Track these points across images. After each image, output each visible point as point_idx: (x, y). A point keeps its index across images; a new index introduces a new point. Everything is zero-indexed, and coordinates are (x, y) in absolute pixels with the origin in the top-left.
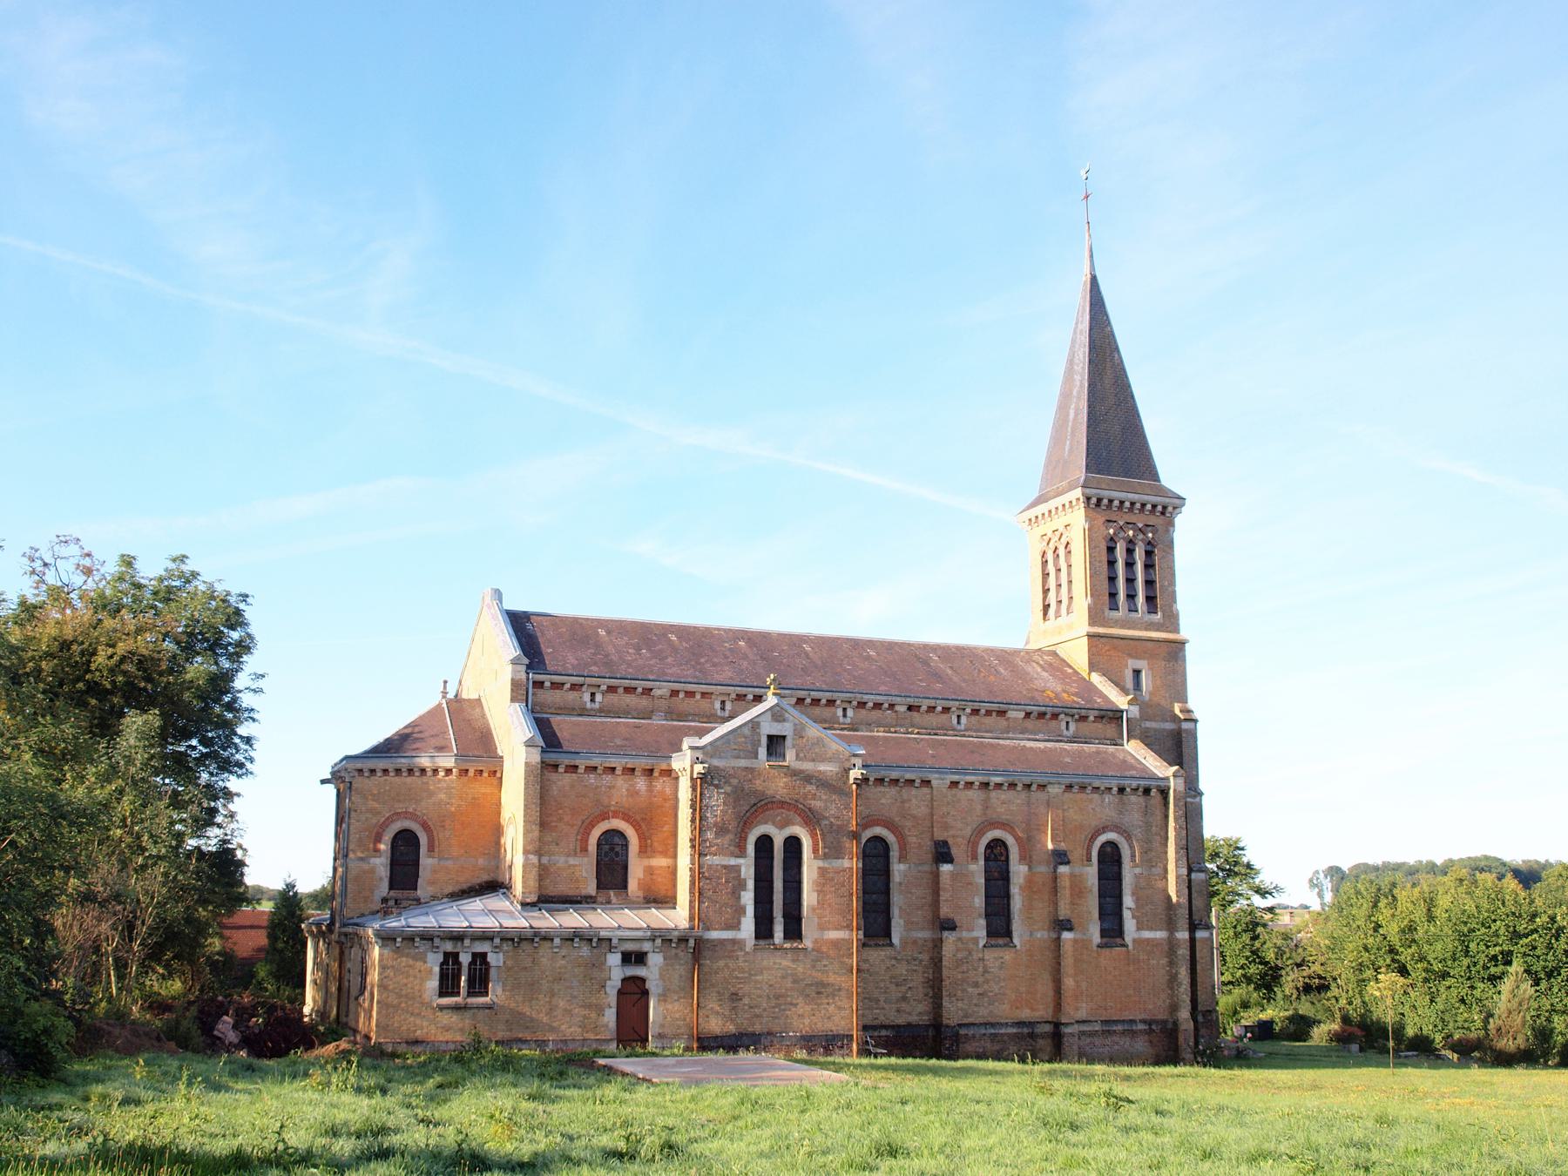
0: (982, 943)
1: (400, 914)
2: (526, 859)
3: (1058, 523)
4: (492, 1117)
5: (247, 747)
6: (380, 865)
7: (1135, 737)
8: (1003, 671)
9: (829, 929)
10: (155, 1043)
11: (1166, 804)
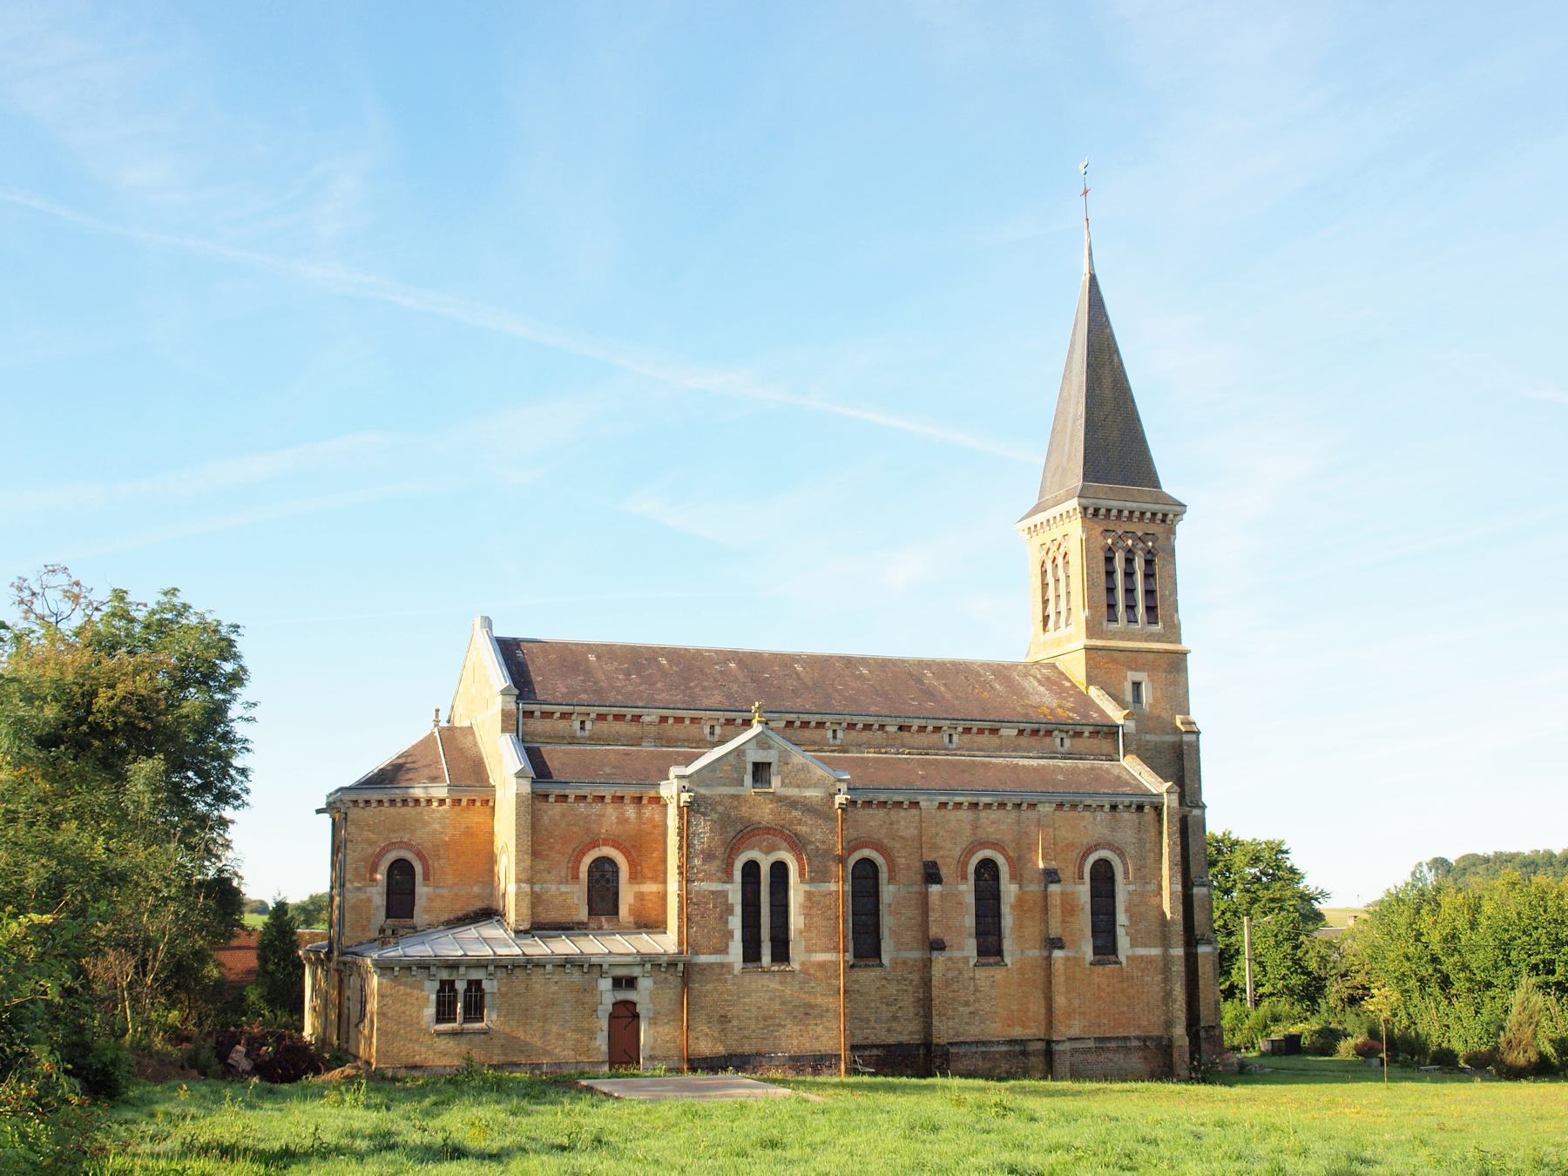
0: (972, 962)
1: (397, 944)
2: (519, 888)
3: (1056, 533)
4: (473, 1124)
5: (243, 778)
6: (377, 895)
7: (1131, 752)
8: (998, 687)
9: (816, 952)
11: (1160, 821)
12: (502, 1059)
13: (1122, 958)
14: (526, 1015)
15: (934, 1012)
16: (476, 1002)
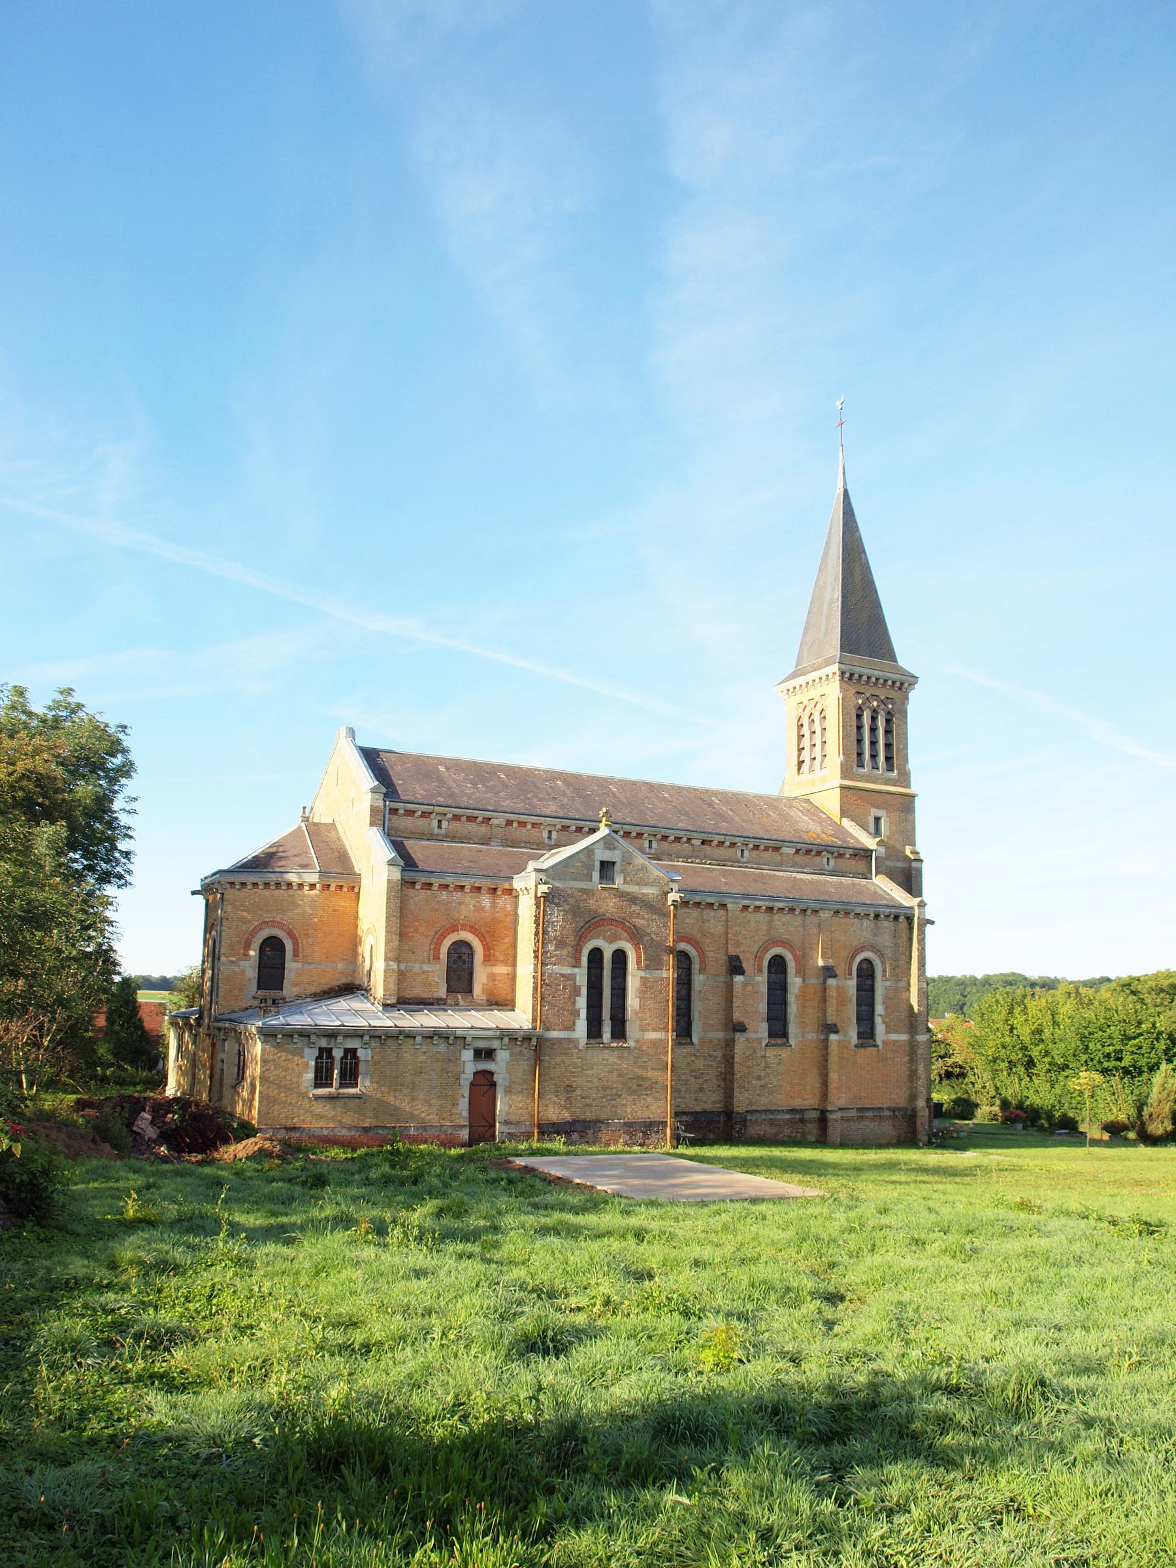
1: (278, 1013)
2: (387, 965)
3: (815, 693)
6: (249, 968)
7: (882, 873)
10: (92, 1146)
12: (374, 1122)
13: (879, 1042)
14: (395, 1084)
15: (735, 1085)
16: (351, 1068)
